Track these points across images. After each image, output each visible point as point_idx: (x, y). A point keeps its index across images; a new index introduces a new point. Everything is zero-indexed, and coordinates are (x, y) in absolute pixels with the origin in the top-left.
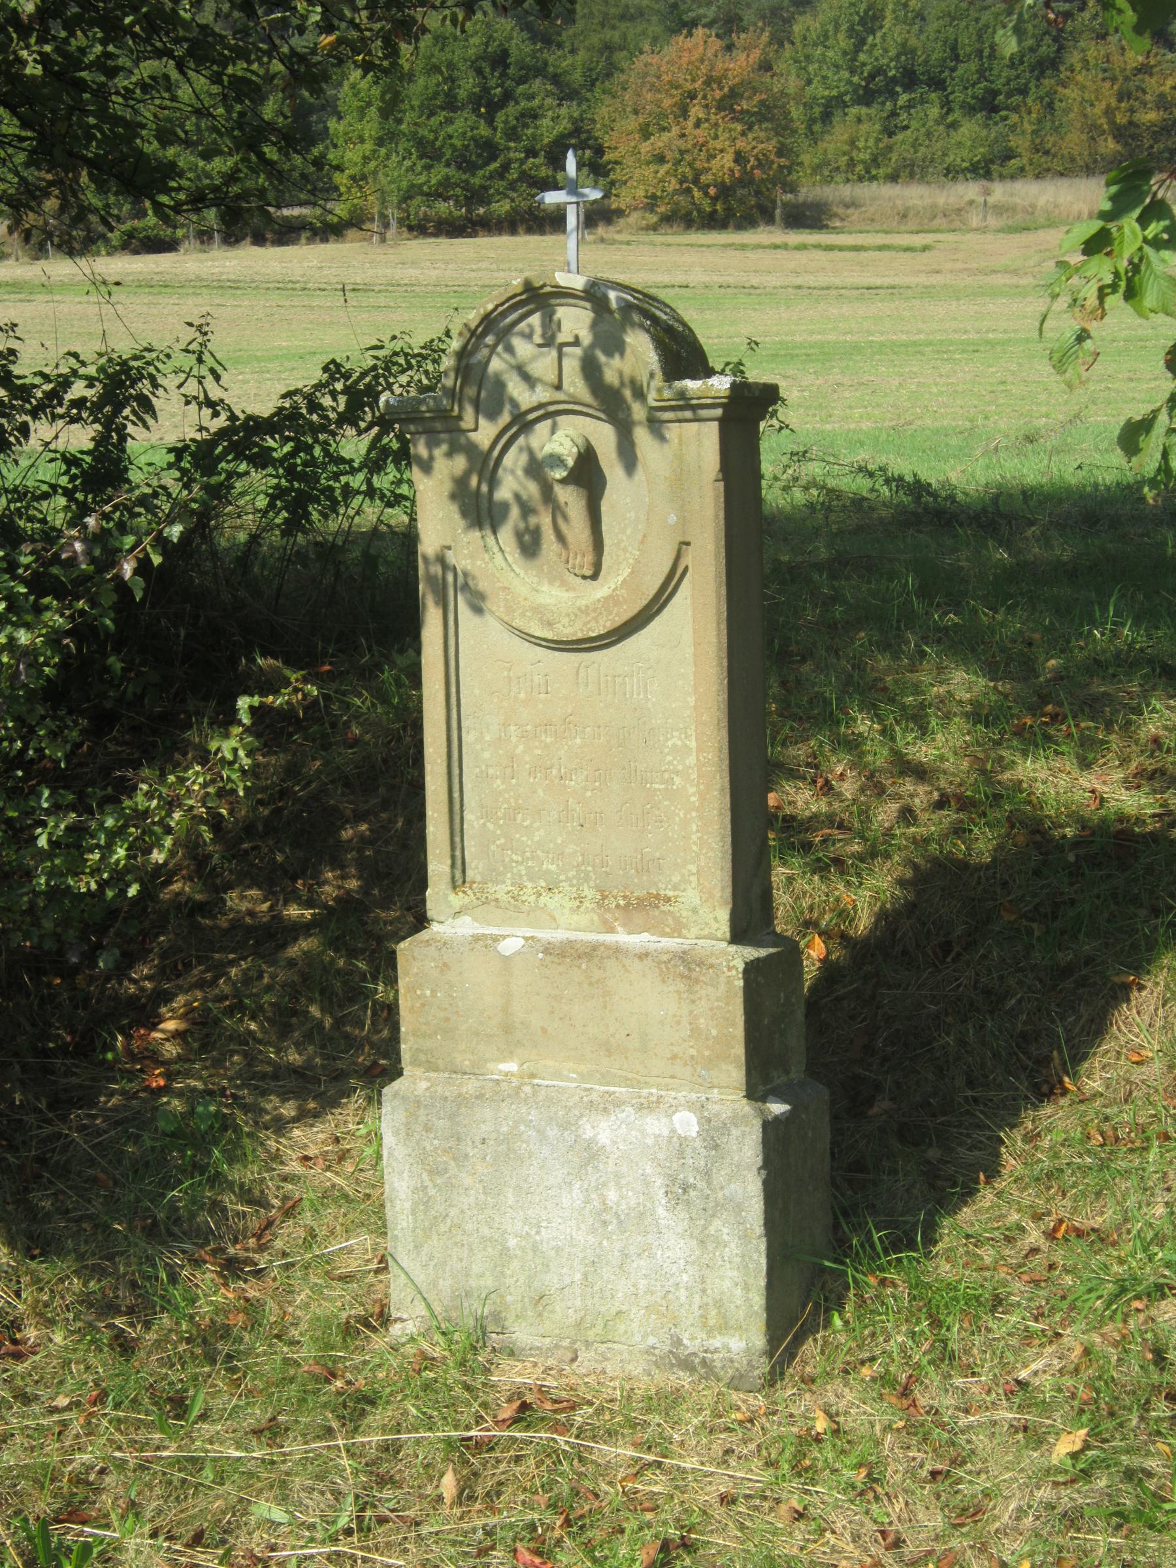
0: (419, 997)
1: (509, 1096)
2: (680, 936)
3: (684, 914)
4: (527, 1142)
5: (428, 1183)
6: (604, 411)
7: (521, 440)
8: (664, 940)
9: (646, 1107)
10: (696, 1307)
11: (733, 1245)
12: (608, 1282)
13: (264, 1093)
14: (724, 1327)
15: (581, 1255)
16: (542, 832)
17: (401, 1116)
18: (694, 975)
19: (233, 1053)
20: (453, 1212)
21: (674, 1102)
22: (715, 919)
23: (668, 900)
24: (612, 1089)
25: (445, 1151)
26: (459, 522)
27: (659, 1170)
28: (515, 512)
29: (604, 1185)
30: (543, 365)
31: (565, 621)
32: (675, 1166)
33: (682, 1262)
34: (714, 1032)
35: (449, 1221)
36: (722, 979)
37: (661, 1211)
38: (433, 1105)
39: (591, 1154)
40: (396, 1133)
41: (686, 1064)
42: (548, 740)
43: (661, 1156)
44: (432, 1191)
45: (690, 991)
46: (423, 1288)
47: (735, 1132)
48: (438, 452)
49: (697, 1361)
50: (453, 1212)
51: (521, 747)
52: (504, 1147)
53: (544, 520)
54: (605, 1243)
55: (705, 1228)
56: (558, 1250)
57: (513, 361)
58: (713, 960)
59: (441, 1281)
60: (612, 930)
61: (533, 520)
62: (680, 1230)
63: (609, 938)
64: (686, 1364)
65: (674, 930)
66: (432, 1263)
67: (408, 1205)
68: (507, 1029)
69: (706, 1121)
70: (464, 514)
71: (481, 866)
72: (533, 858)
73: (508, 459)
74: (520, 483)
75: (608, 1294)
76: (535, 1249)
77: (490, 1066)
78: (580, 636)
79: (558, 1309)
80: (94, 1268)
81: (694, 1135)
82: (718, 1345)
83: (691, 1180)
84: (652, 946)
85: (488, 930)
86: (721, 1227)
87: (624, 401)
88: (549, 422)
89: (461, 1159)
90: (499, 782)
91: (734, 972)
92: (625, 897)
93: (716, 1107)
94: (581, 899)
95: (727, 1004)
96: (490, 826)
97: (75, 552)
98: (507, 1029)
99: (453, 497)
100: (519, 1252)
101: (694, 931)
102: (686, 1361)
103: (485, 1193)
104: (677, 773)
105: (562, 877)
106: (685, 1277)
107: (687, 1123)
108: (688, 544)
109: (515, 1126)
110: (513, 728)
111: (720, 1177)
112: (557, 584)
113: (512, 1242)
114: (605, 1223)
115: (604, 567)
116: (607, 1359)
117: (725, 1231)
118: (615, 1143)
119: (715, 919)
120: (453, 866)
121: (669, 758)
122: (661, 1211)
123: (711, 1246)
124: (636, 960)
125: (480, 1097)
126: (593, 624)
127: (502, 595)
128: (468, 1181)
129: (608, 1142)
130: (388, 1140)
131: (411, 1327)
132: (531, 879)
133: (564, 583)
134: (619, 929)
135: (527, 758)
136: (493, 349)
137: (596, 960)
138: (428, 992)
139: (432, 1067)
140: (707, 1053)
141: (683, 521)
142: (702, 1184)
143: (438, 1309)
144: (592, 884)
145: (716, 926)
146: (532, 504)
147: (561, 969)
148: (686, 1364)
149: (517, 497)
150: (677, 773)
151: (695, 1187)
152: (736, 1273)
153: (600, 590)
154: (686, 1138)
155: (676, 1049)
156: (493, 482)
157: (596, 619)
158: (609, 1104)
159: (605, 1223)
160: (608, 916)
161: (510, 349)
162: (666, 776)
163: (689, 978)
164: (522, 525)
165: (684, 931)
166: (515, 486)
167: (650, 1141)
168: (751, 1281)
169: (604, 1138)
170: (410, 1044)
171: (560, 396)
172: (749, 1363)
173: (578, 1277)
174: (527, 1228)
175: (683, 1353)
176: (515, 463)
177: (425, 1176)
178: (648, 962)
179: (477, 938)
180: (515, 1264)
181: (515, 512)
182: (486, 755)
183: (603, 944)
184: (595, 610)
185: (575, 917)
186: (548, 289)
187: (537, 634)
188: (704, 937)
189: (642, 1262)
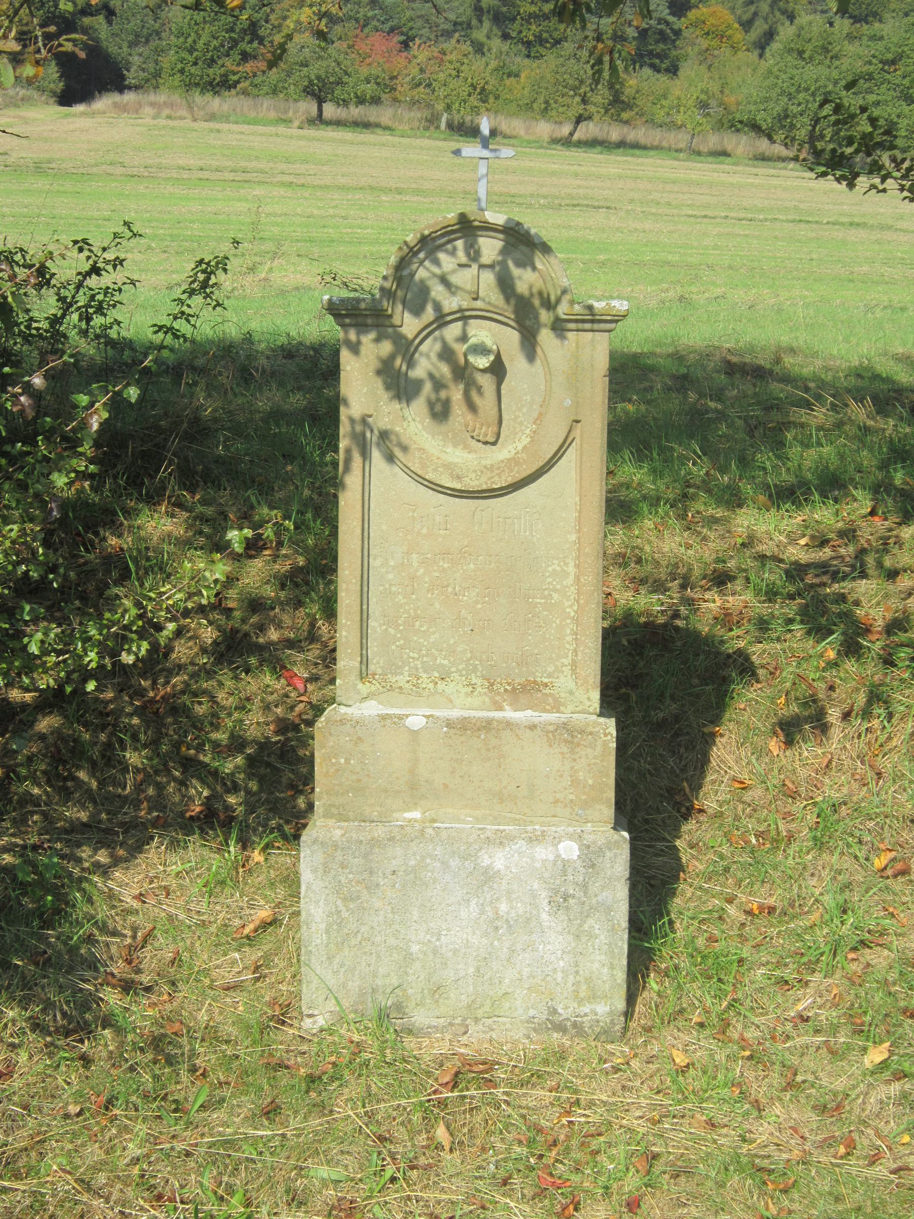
0: (334, 764)
1: (416, 837)
2: (558, 712)
3: (563, 695)
4: (432, 872)
5: (342, 908)
6: (517, 322)
7: (437, 333)
9: (533, 840)
10: (569, 984)
11: (602, 937)
12: (497, 972)
13: (79, 845)
14: (593, 997)
15: (475, 954)
16: (437, 635)
17: (319, 857)
18: (576, 740)
19: (32, 813)
20: (363, 929)
21: (556, 835)
22: (589, 699)
23: (546, 685)
24: (502, 828)
25: (358, 882)
26: (384, 395)
27: (544, 885)
28: (428, 387)
29: (498, 899)
30: (464, 278)
31: (473, 476)
32: (558, 882)
33: (559, 953)
35: (359, 936)
36: (599, 743)
37: (544, 916)
39: (488, 877)
40: (314, 871)
41: (566, 806)
42: (446, 565)
43: (547, 875)
44: (345, 914)
45: (572, 752)
46: (334, 989)
47: (609, 854)
49: (569, 1024)
50: (363, 929)
51: (422, 571)
52: (412, 876)
53: (456, 394)
54: (496, 943)
56: (455, 951)
57: (437, 270)
58: (590, 729)
59: (350, 983)
60: (501, 709)
61: (443, 394)
62: (560, 929)
64: (561, 1028)
65: (553, 708)
66: (343, 970)
67: (323, 926)
68: (413, 786)
69: (586, 848)
70: (388, 388)
71: (382, 662)
72: (427, 656)
73: (424, 348)
74: (433, 364)
75: (497, 981)
76: (435, 952)
77: (396, 815)
78: (484, 487)
80: (24, 998)
81: (575, 858)
82: (587, 1010)
83: (571, 892)
84: (536, 720)
85: (391, 711)
88: (460, 323)
89: (373, 888)
90: (400, 597)
91: (609, 737)
92: (509, 684)
93: (592, 837)
94: (474, 686)
95: (602, 761)
96: (391, 631)
97: (22, 405)
98: (413, 786)
100: (421, 956)
101: (571, 708)
102: (560, 1025)
104: (556, 591)
105: (453, 669)
106: (561, 963)
107: (570, 850)
108: (577, 422)
109: (423, 858)
111: (594, 888)
112: (461, 447)
113: (415, 948)
114: (497, 928)
115: (502, 435)
116: (493, 1030)
117: (597, 927)
118: (507, 867)
119: (589, 699)
120: (361, 662)
121: (550, 580)
122: (544, 916)
123: (584, 939)
124: (528, 731)
125: (391, 839)
126: (496, 479)
127: (417, 454)
128: (378, 904)
129: (502, 867)
130: (306, 875)
131: (321, 1021)
132: (425, 672)
133: (466, 447)
134: (507, 707)
135: (427, 579)
136: (421, 263)
137: (493, 732)
138: (342, 761)
139: (342, 818)
140: (583, 797)
142: (579, 894)
143: (346, 1004)
144: (479, 674)
145: (588, 703)
147: (462, 739)
148: (561, 1028)
151: (573, 896)
152: (603, 957)
153: (502, 453)
154: (568, 861)
155: (558, 796)
156: (411, 363)
157: (499, 475)
158: (502, 840)
159: (497, 928)
160: (498, 698)
161: (437, 262)
162: (546, 593)
163: (572, 743)
164: (433, 397)
165: (562, 708)
166: (430, 367)
167: (538, 865)
168: (616, 962)
169: (499, 864)
171: (479, 304)
172: (612, 1022)
173: (471, 970)
174: (428, 937)
176: (430, 350)
177: (339, 902)
178: (538, 731)
179: (384, 717)
180: (418, 965)
182: (391, 576)
183: (493, 719)
184: (498, 468)
185: (469, 700)
186: (476, 223)
188: (579, 712)
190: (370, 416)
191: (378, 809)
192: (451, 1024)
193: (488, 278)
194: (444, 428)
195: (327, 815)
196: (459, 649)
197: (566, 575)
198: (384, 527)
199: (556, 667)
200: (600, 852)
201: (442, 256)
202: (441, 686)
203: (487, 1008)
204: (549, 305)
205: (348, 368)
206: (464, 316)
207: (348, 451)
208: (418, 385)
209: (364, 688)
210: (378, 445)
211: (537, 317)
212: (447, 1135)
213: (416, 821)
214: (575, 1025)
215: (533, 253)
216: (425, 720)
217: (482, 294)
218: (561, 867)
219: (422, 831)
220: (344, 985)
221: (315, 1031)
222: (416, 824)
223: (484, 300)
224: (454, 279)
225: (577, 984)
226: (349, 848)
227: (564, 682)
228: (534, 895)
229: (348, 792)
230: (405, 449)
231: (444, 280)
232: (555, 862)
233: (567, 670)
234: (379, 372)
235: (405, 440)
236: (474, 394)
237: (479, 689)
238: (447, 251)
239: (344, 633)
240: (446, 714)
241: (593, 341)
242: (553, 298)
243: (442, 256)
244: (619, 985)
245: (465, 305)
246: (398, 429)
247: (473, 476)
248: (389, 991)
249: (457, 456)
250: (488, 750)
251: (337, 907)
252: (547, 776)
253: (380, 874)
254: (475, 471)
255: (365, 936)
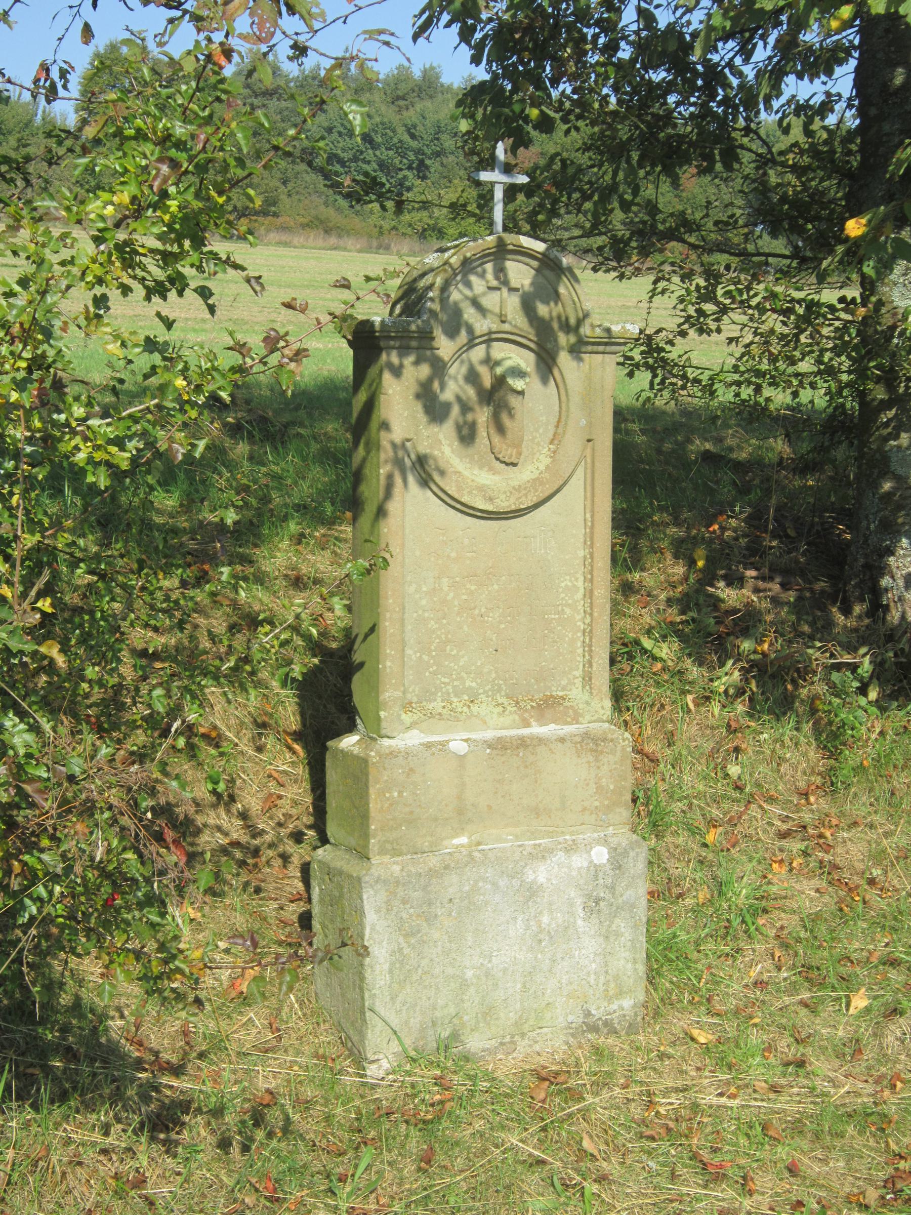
0: (388, 799)
3: (581, 706)
5: (404, 945)
8: (565, 727)
9: (571, 848)
10: (601, 985)
11: (627, 935)
14: (620, 994)
16: (466, 658)
17: (383, 896)
18: (600, 748)
20: (424, 962)
22: (603, 708)
25: (418, 916)
28: (456, 410)
29: (541, 913)
30: (491, 301)
31: (503, 497)
33: (592, 956)
34: (612, 787)
35: (420, 970)
36: (619, 748)
37: (580, 922)
38: (409, 882)
39: (532, 891)
40: (378, 911)
43: (582, 882)
44: (406, 951)
45: (597, 760)
47: (632, 854)
48: (409, 360)
51: (451, 595)
53: (482, 416)
54: (539, 956)
55: (609, 926)
56: (505, 970)
57: (468, 293)
60: (528, 725)
61: (470, 417)
62: (593, 932)
63: (525, 732)
64: (594, 1029)
67: (386, 966)
74: (460, 386)
76: (487, 974)
77: (445, 843)
78: (513, 508)
79: (502, 1015)
81: (605, 861)
83: (602, 895)
86: (620, 924)
87: (552, 329)
88: (484, 346)
96: (425, 658)
99: (418, 396)
100: (474, 981)
101: (588, 718)
103: (450, 942)
104: (569, 605)
107: (600, 855)
109: (476, 882)
110: (445, 580)
113: (469, 974)
114: (540, 941)
116: (536, 1042)
118: (549, 880)
119: (603, 708)
121: (563, 595)
122: (580, 922)
123: (612, 939)
124: (560, 744)
125: (447, 867)
126: (523, 499)
128: (436, 935)
132: (456, 696)
133: (491, 469)
134: (534, 723)
138: (396, 794)
139: (396, 853)
140: (606, 803)
141: (590, 425)
142: (608, 896)
143: (408, 1042)
144: (503, 693)
146: (470, 404)
147: (503, 759)
148: (594, 1029)
149: (459, 399)
150: (569, 605)
152: (628, 953)
157: (526, 495)
158: (542, 854)
160: (526, 715)
161: (468, 285)
163: (596, 751)
166: (457, 390)
167: (574, 873)
168: (638, 956)
169: (542, 879)
170: (378, 838)
171: (506, 327)
172: (636, 1015)
173: (519, 986)
175: (591, 1020)
176: (458, 373)
177: (401, 940)
178: (568, 744)
179: (428, 746)
180: (472, 990)
181: (456, 410)
182: (424, 602)
185: (502, 719)
186: (511, 247)
187: (481, 507)
189: (565, 963)
190: (408, 440)
191: (429, 839)
192: (502, 1044)
193: (513, 303)
194: (470, 451)
195: (382, 852)
196: (486, 670)
197: (577, 589)
198: (418, 553)
199: (569, 679)
200: (625, 853)
201: (473, 278)
202: (474, 708)
203: (531, 1022)
204: (567, 327)
205: (390, 391)
206: (490, 339)
207: (390, 477)
208: (447, 406)
209: (407, 718)
210: (412, 470)
211: (556, 340)
212: (593, 1145)
213: (463, 846)
214: (606, 1023)
215: (559, 278)
216: (465, 744)
217: (509, 317)
218: (593, 873)
219: (470, 855)
220: (407, 1023)
221: (381, 1076)
222: (463, 849)
223: (510, 323)
224: (485, 302)
225: (606, 983)
226: (409, 882)
227: (577, 694)
228: (572, 904)
229: (401, 825)
230: (442, 473)
231: (475, 303)
232: (589, 868)
233: (578, 682)
234: (418, 396)
235: (442, 465)
236: (505, 417)
237: (509, 708)
238: (477, 274)
239: (388, 664)
240: (481, 736)
241: (603, 362)
242: (572, 321)
243: (473, 278)
244: (641, 978)
245: (494, 327)
246: (436, 453)
247: (503, 497)
248: (447, 1021)
249: (484, 478)
250: (526, 767)
251: (399, 944)
252: (576, 787)
253: (438, 904)
254: (505, 492)
255: (426, 969)
